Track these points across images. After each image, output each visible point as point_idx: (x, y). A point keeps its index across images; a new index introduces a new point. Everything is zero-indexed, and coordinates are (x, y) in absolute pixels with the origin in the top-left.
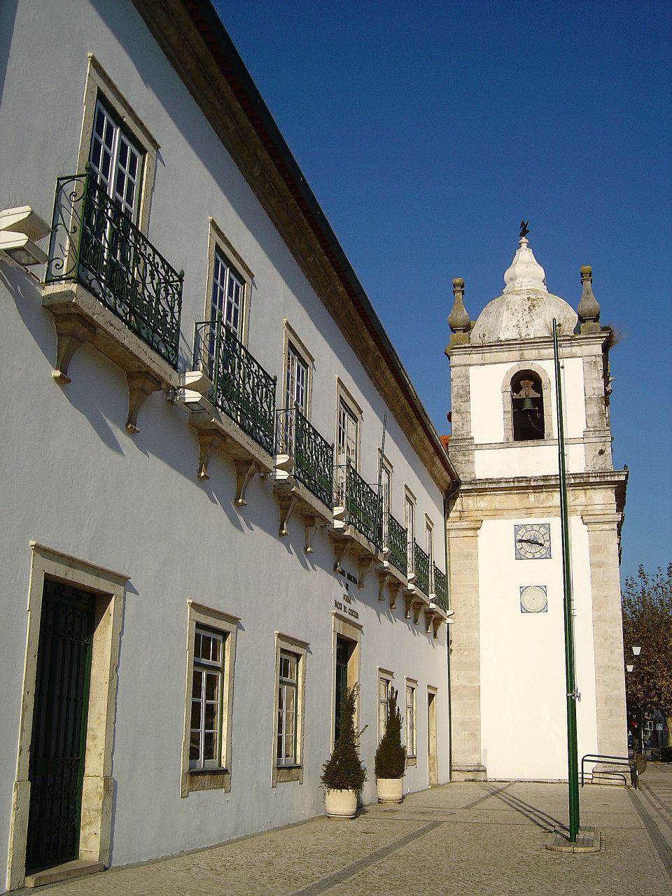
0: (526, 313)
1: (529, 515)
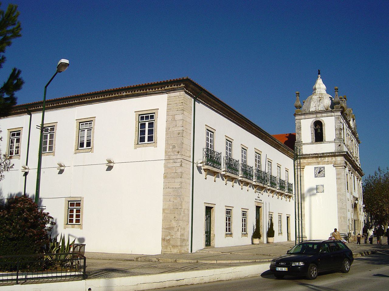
0: (318, 102)
1: (319, 164)
